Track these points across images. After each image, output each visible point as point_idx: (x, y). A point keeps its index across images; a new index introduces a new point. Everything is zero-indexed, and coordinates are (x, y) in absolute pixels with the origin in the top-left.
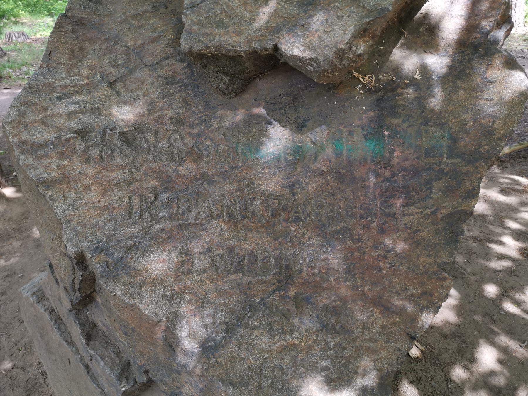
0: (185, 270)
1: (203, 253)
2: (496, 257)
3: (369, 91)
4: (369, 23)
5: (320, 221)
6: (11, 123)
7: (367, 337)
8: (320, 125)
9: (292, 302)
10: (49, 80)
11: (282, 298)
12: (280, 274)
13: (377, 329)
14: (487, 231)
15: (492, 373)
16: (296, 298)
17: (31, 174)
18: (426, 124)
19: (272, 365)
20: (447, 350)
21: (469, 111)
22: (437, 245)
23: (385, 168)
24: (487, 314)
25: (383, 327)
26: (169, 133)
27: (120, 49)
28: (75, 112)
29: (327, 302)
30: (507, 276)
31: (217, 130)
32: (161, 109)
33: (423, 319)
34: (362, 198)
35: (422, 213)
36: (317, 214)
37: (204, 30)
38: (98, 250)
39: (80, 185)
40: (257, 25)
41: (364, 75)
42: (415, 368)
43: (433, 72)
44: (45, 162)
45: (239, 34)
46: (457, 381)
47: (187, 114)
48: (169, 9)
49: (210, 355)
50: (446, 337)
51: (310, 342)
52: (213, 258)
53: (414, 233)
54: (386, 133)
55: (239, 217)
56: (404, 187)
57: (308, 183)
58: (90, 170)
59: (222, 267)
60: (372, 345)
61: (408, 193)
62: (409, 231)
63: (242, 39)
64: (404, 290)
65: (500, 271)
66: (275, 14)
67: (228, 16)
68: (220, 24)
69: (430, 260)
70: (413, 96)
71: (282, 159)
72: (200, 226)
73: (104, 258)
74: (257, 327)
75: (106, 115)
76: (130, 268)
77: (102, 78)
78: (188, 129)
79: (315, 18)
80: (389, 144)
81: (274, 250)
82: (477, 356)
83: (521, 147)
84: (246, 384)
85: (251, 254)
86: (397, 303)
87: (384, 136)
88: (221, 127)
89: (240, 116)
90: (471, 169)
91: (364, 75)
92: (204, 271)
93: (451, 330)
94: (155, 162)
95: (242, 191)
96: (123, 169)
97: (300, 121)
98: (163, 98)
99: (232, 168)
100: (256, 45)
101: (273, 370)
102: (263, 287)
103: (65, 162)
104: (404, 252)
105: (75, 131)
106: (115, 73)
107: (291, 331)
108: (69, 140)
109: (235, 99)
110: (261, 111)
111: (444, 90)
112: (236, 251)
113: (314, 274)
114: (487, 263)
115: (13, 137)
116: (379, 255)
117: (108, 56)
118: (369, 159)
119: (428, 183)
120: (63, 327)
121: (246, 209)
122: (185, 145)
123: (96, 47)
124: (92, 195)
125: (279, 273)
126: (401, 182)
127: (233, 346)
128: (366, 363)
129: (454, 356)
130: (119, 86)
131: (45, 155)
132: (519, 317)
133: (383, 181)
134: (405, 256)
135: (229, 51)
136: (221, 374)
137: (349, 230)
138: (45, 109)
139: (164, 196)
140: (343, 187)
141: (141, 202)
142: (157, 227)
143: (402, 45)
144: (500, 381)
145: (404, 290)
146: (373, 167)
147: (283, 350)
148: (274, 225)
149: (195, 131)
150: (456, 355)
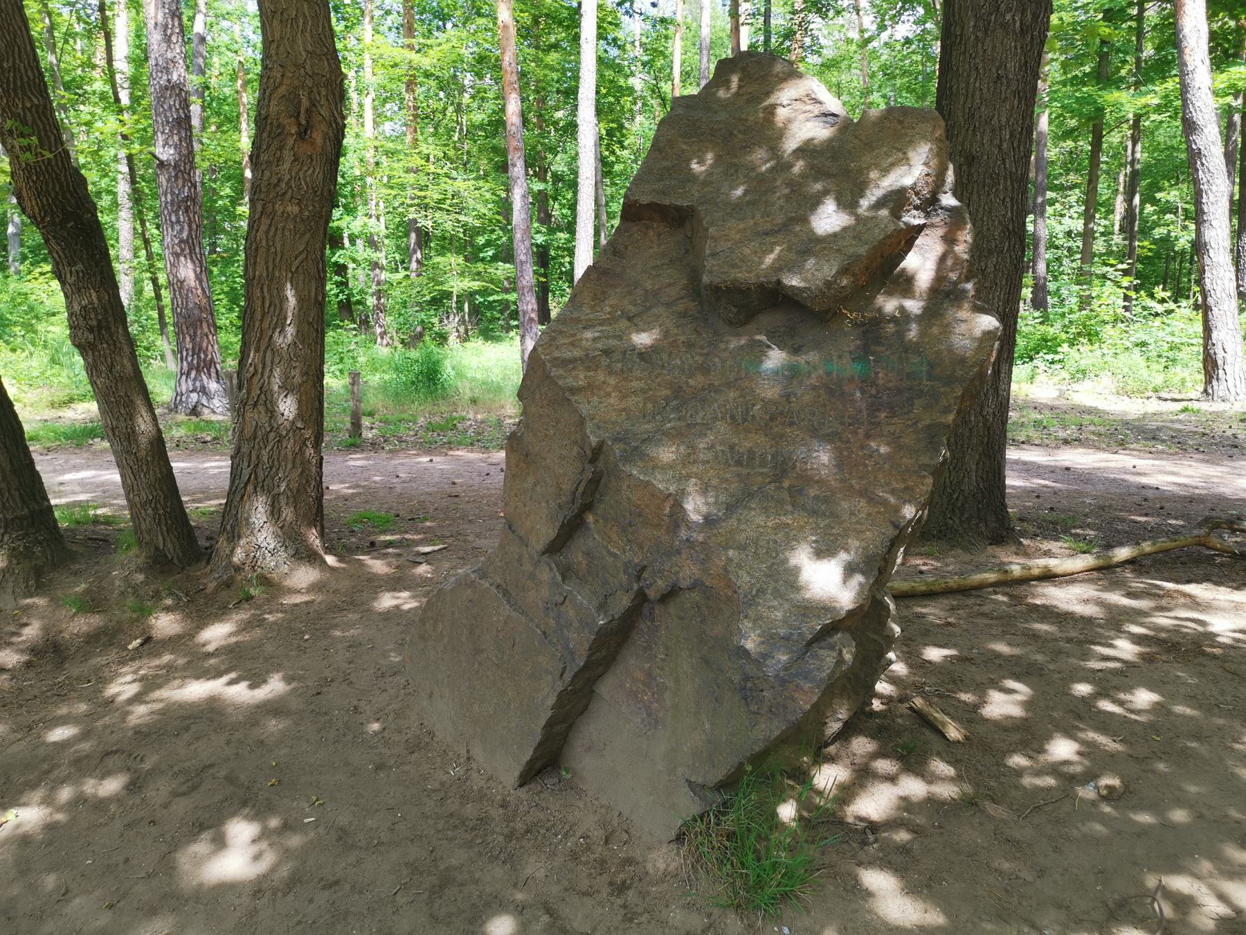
1: (708, 449)
3: (856, 325)
8: (813, 350)
10: (576, 315)
14: (1092, 634)
15: (1067, 763)
16: (789, 489)
18: (906, 352)
23: (871, 386)
25: (869, 515)
27: (639, 292)
28: (599, 338)
29: (818, 493)
32: (676, 335)
38: (616, 440)
40: (763, 266)
45: (750, 272)
50: (1005, 729)
58: (612, 381)
61: (892, 408)
63: (752, 275)
64: (888, 484)
66: (779, 258)
68: (734, 266)
71: (780, 374)
76: (644, 455)
83: (1174, 544)
84: (745, 549)
85: (750, 451)
87: (870, 360)
88: (727, 348)
90: (948, 389)
91: (851, 313)
92: (708, 462)
98: (677, 327)
99: (736, 380)
102: (760, 479)
103: (591, 373)
104: (888, 454)
108: (595, 357)
119: (910, 399)
121: (747, 413)
123: (618, 290)
127: (733, 522)
131: (574, 368)
132: (1119, 715)
134: (889, 457)
138: (575, 335)
140: (833, 400)
142: (669, 425)
143: (884, 293)
145: (888, 484)
147: (777, 528)
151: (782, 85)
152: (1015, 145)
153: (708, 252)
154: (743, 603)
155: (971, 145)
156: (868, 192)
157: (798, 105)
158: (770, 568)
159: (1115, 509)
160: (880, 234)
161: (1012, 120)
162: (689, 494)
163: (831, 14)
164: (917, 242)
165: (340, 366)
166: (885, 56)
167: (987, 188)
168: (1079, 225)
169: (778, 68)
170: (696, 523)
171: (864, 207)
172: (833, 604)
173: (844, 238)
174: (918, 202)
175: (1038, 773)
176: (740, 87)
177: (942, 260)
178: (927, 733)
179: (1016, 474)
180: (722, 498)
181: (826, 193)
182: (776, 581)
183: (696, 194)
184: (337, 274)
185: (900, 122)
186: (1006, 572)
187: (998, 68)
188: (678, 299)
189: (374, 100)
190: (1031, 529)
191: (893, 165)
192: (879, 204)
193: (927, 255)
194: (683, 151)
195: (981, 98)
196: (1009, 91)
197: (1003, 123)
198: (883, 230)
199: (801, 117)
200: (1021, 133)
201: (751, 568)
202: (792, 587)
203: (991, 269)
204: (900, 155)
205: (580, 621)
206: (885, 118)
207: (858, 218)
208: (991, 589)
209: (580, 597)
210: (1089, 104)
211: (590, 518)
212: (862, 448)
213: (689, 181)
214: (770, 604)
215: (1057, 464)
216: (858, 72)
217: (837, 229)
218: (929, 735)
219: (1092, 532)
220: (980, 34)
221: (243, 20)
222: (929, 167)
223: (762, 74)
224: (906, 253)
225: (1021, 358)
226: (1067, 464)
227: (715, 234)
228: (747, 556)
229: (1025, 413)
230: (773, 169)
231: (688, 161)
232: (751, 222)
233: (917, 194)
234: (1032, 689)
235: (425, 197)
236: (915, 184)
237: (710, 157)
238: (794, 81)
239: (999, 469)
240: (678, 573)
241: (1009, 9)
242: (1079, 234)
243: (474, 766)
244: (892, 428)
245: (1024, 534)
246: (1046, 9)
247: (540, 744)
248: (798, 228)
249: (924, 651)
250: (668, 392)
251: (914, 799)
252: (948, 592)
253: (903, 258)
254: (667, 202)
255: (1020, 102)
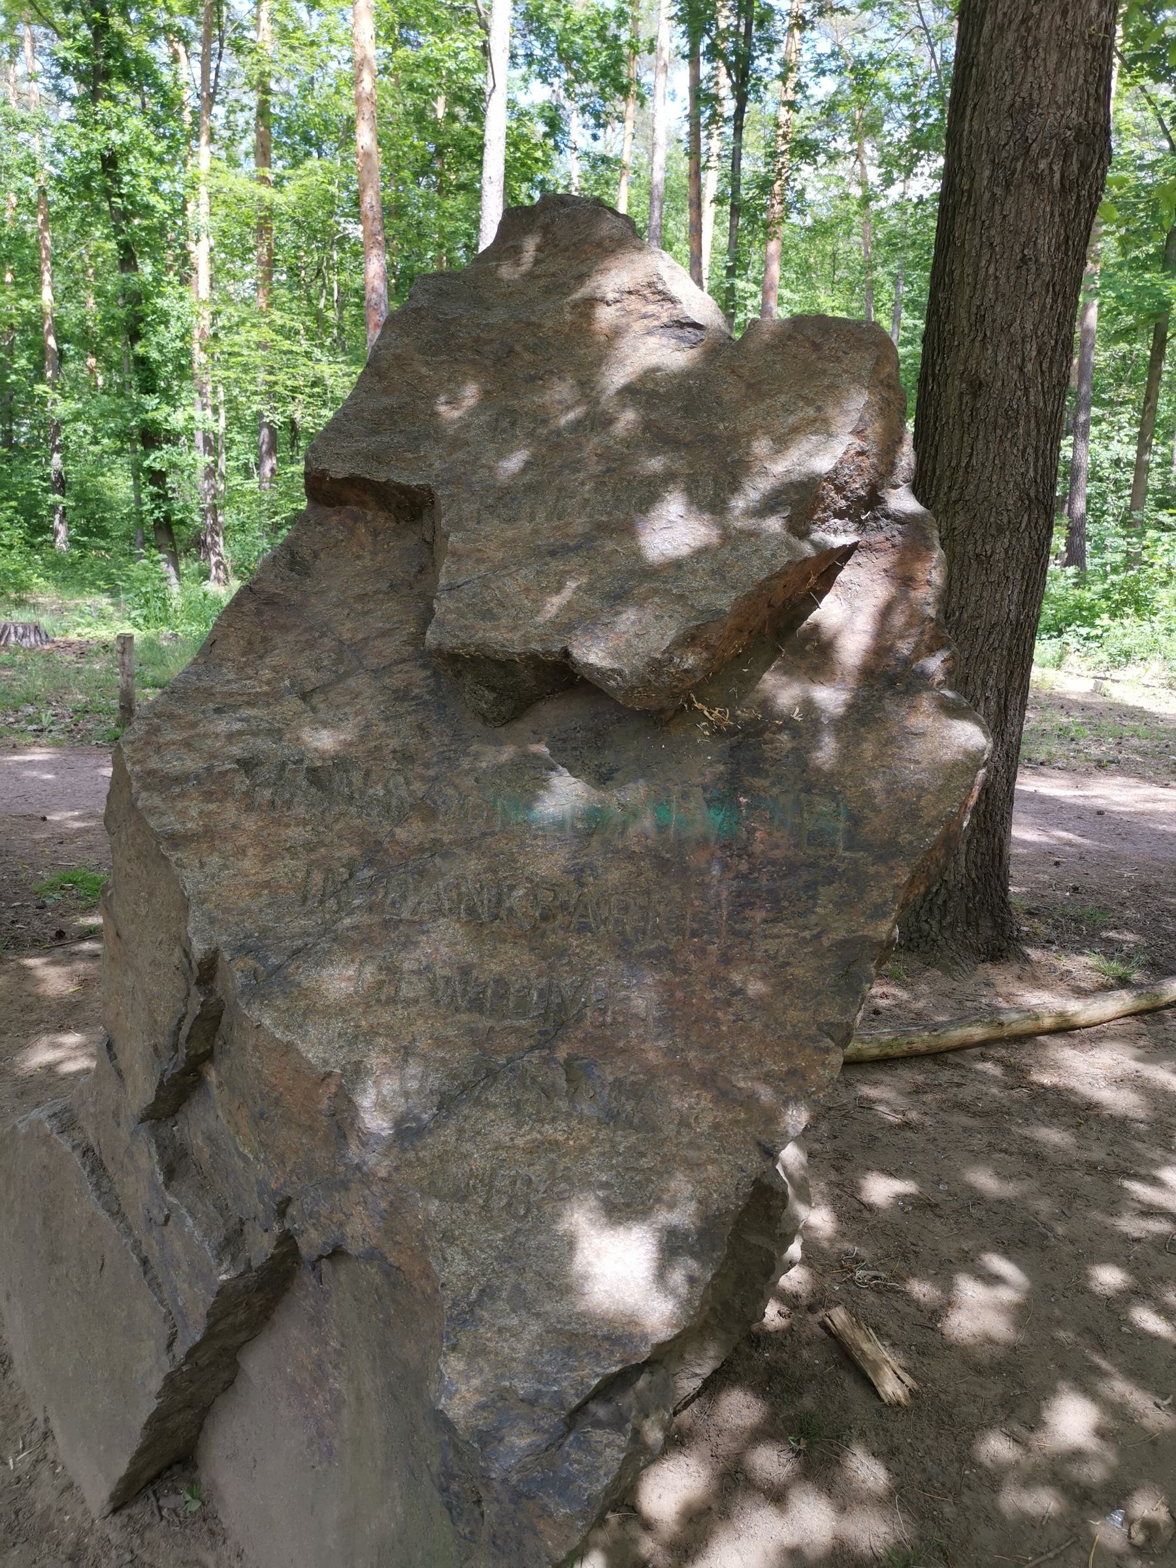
0: (383, 998)
1: (419, 972)
2: (1134, 1209)
3: (717, 732)
4: (698, 627)
5: (621, 933)
6: (132, 743)
7: (685, 1140)
8: (635, 781)
9: (562, 1071)
10: (206, 682)
11: (546, 1061)
12: (545, 1020)
13: (704, 1127)
14: (1127, 1154)
15: (1077, 1455)
16: (568, 1064)
17: (153, 822)
18: (808, 791)
19: (513, 1173)
20: (974, 1398)
21: (880, 776)
22: (819, 992)
23: (740, 856)
24: (1089, 1330)
25: (716, 1126)
26: (387, 774)
28: (240, 733)
29: (621, 1075)
30: (1152, 1252)
31: (467, 773)
32: (381, 736)
33: (788, 1119)
34: (696, 903)
35: (796, 936)
36: (617, 921)
37: (463, 622)
38: (243, 950)
39: (229, 846)
40: (540, 619)
41: (711, 707)
42: (890, 1425)
43: (823, 711)
44: (179, 805)
45: (515, 628)
46: (988, 1463)
47: (423, 747)
48: (416, 591)
49: (406, 1144)
50: (978, 1370)
51: (585, 1141)
52: (433, 981)
53: (781, 967)
54: (743, 800)
55: (485, 917)
56: (770, 891)
57: (607, 870)
58: (250, 823)
59: (446, 1000)
60: (692, 1154)
61: (777, 901)
62: (772, 963)
63: (516, 636)
64: (757, 1063)
65: (1138, 1240)
66: (569, 606)
67: (501, 604)
68: (488, 615)
69: (806, 1016)
70: (789, 745)
71: (568, 827)
72: (417, 924)
73: (252, 963)
74: (495, 1106)
75: (290, 741)
77: (293, 685)
78: (420, 770)
79: (624, 616)
80: (747, 818)
81: (538, 977)
82: (1046, 1415)
85: (499, 981)
86: (742, 1084)
87: (739, 805)
89: (507, 753)
90: (883, 869)
91: (711, 707)
92: (416, 1001)
93: (992, 1357)
94: (359, 817)
95: (495, 872)
96: (305, 825)
97: (603, 770)
98: (387, 719)
100: (535, 646)
101: (514, 1183)
102: (513, 1040)
103: (212, 807)
104: (761, 998)
105: (238, 761)
106: (312, 677)
107: (554, 1120)
108: (224, 774)
109: (503, 729)
110: (543, 749)
111: (838, 739)
112: (475, 973)
113: (603, 1024)
114: (1110, 1221)
115: (134, 764)
116: (716, 998)
117: (307, 652)
118: (713, 839)
119: (811, 886)
120: (105, 1182)
121: (499, 902)
122: (411, 793)
123: (290, 638)
124: (247, 864)
125: (544, 1017)
126: (765, 882)
127: (449, 1134)
128: (680, 1184)
129: (990, 1411)
130: (317, 699)
131: (182, 795)
133: (736, 877)
134: (759, 1005)
135: (496, 652)
136: (421, 1179)
137: (670, 952)
138: (194, 725)
139: (367, 873)
141: (326, 880)
142: (347, 921)
144: (1095, 1473)
145: (757, 1063)
146: (719, 853)
147: (534, 1150)
148: (544, 935)
149: (431, 772)
150: (995, 1412)
151: (606, 264)
152: (1045, 366)
153: (443, 581)
154: (450, 1319)
155: (978, 363)
156: (747, 486)
157: (633, 303)
158: (509, 1240)
159: (1165, 892)
160: (761, 569)
161: (1042, 328)
162: (369, 1072)
163: (821, 158)
164: (842, 576)
165: (145, 612)
166: (894, 219)
167: (999, 432)
168: (1130, 452)
169: (606, 228)
170: (378, 1138)
171: (737, 512)
172: (631, 1329)
173: (694, 572)
174: (843, 503)
175: (1028, 1481)
176: (537, 262)
177: (886, 612)
178: (848, 1382)
179: (1030, 819)
180: (434, 1081)
181: (668, 478)
182: (521, 1271)
183: (437, 464)
184: (152, 482)
185: (816, 347)
186: (1001, 1024)
187: (1024, 246)
188: (396, 663)
189: (211, 250)
190: (1042, 929)
191: (795, 430)
192: (768, 506)
193: (857, 603)
194: (421, 378)
195: (996, 292)
196: (1038, 283)
197: (1028, 332)
198: (767, 561)
199: (638, 326)
200: (1054, 349)
201: (473, 1241)
202: (550, 1286)
203: (1000, 554)
204: (811, 412)
205: (191, 1265)
206: (790, 337)
207: (728, 537)
208: (976, 1051)
209: (190, 1221)
210: (1151, 296)
211: (212, 1076)
212: (713, 983)
213: (428, 436)
214: (503, 1322)
215: (1086, 802)
216: (859, 239)
217: (685, 551)
218: (852, 1389)
219: (1130, 937)
220: (999, 191)
221: (44, 131)
222: (865, 439)
223: (575, 239)
224: (821, 595)
225: (1048, 629)
226: (1100, 803)
227: (460, 546)
228: (467, 1213)
229: (1048, 715)
230: (577, 425)
231: (432, 397)
232: (528, 527)
233: (839, 489)
234: (1028, 1276)
235: (276, 383)
236: (835, 470)
237: (471, 393)
238: (628, 257)
239: (1001, 850)
240: (341, 1225)
241: (1044, 153)
242: (1129, 464)
243: (50, 1451)
244: (771, 946)
245: (1032, 939)
246: (1101, 158)
247: (140, 1453)
248: (610, 546)
249: (862, 1181)
250: (354, 851)
251: (811, 1554)
252: (912, 1058)
253: (814, 605)
254: (381, 477)
255: (1055, 301)
